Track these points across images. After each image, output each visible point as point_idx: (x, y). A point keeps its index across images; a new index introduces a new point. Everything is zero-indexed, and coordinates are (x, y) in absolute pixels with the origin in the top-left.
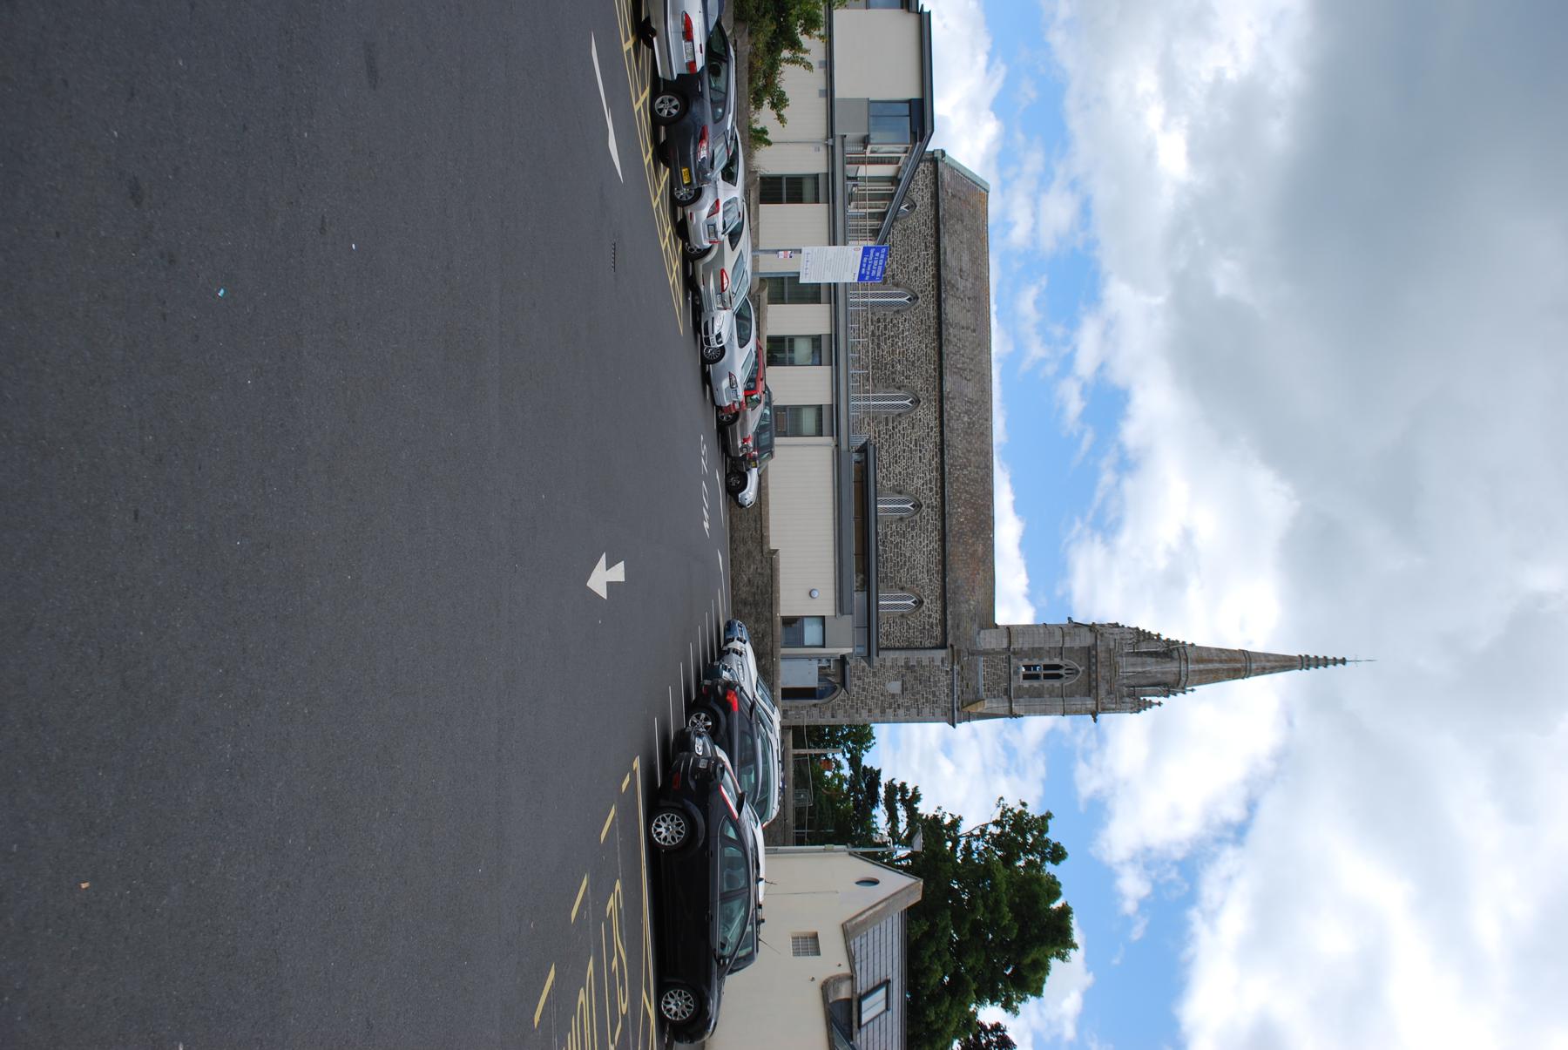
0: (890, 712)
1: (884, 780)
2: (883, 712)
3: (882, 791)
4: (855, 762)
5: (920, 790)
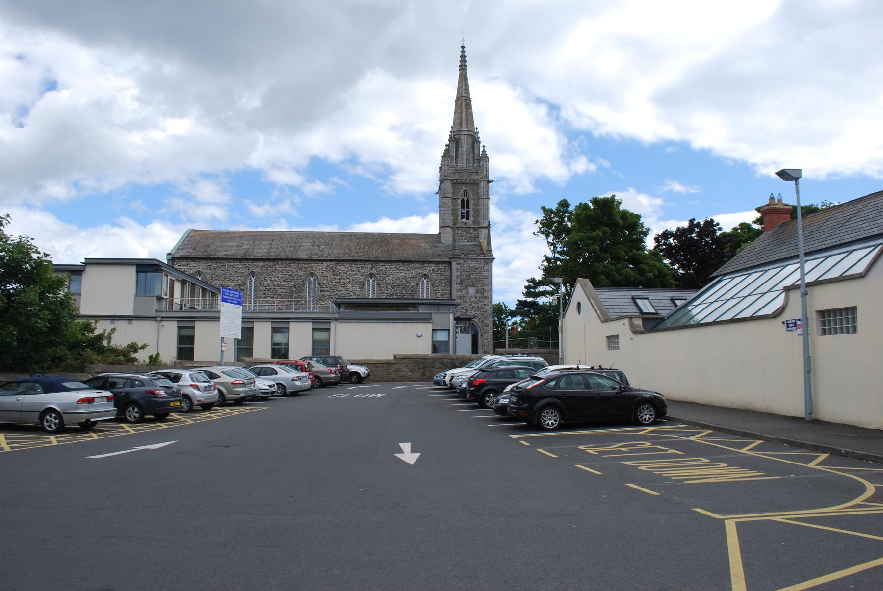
1: (523, 298)
2: (486, 298)
3: (529, 299)
4: (513, 314)
5: (529, 278)
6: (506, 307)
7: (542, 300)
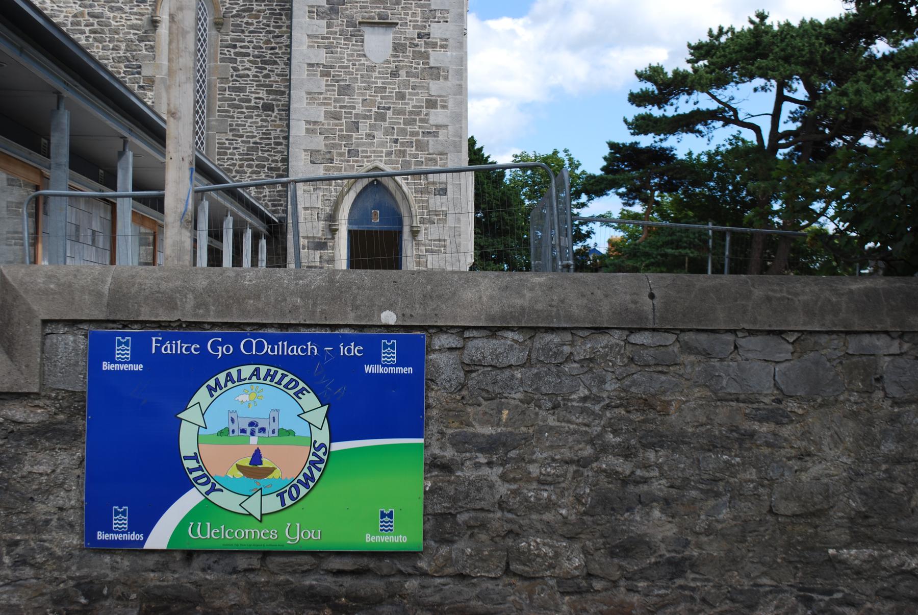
0: (436, 58)
1: (625, 137)
2: (436, 73)
3: (646, 141)
4: (595, 187)
5: (642, 67)
6: (574, 165)
7: (685, 146)
